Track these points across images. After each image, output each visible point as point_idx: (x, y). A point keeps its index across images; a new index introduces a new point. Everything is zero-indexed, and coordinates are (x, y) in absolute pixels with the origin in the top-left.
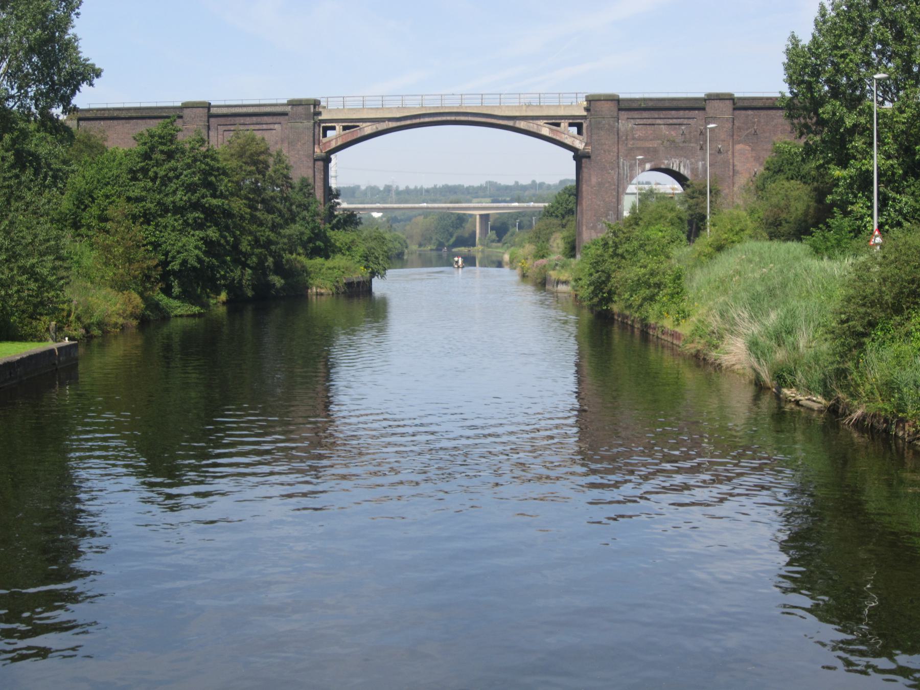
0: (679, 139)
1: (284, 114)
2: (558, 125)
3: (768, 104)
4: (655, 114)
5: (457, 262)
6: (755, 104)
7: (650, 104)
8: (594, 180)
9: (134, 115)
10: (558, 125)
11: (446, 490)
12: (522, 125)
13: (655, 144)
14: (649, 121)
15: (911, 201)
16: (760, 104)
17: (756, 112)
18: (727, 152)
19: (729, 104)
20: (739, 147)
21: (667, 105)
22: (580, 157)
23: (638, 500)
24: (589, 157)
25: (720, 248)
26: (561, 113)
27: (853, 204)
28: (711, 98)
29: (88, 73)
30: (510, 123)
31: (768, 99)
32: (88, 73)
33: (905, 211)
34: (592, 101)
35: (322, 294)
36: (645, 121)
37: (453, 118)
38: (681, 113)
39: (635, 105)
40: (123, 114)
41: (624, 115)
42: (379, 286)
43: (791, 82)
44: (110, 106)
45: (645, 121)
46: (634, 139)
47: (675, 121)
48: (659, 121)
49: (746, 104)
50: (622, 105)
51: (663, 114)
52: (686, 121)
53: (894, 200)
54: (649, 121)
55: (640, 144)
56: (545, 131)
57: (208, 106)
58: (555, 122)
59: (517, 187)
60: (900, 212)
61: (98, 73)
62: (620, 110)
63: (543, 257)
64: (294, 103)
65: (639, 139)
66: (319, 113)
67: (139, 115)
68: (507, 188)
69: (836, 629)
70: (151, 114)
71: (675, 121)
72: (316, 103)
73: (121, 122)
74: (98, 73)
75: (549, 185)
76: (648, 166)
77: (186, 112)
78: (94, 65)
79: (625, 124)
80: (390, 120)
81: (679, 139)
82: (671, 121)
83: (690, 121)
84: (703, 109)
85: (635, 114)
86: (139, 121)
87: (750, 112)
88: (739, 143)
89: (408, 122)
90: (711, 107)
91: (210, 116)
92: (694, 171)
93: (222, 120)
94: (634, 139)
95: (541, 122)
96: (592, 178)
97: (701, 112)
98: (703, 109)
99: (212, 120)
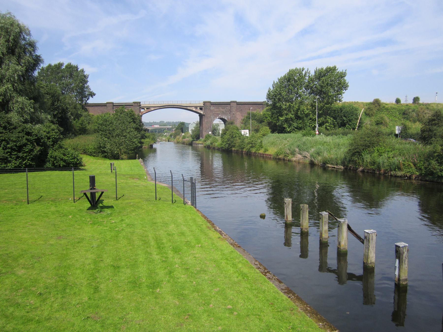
0: (225, 111)
1: (132, 105)
2: (197, 108)
3: (244, 103)
4: (219, 106)
5: (158, 141)
6: (241, 103)
7: (218, 103)
8: (206, 121)
9: (94, 105)
10: (197, 108)
11: (261, 194)
12: (189, 108)
13: (219, 112)
14: (218, 107)
15: (297, 124)
16: (252, 103)
17: (242, 105)
18: (235, 114)
19: (236, 103)
20: (238, 113)
21: (222, 103)
22: (201, 116)
23: (242, 193)
24: (204, 115)
25: (264, 135)
26: (198, 105)
27: (284, 125)
28: (232, 102)
29: (92, 94)
30: (186, 108)
31: (244, 102)
32: (92, 94)
33: (295, 127)
34: (205, 103)
35: (146, 148)
36: (217, 107)
37: (173, 106)
38: (225, 105)
39: (215, 104)
40: (91, 105)
41: (212, 106)
42: (155, 146)
43: (269, 96)
44: (94, 103)
45: (217, 107)
46: (214, 111)
47: (224, 107)
48: (220, 107)
49: (239, 103)
50: (212, 104)
51: (221, 106)
52: (226, 107)
53: (293, 124)
54: (218, 107)
55: (216, 112)
56: (194, 110)
57: (113, 103)
58: (196, 107)
59: (150, 123)
60: (294, 127)
61: (94, 95)
62: (211, 105)
63: (184, 138)
64: (134, 103)
65: (216, 111)
66: (141, 105)
67: (95, 105)
68: (148, 123)
69: (425, 225)
70: (98, 105)
71: (224, 107)
72: (140, 103)
73: (91, 107)
74: (94, 95)
75: (157, 122)
76: (218, 117)
77: (107, 104)
78: (94, 93)
79: (212, 108)
80: (158, 107)
81: (225, 111)
82: (223, 107)
83: (227, 107)
84: (230, 104)
85: (215, 106)
86: (96, 107)
87: (240, 105)
88: (238, 112)
89: (162, 107)
90: (231, 104)
91: (114, 106)
92: (228, 118)
93: (117, 107)
94: (214, 111)
95: (193, 108)
96: (205, 120)
97: (230, 105)
98: (230, 104)
99: (114, 107)
